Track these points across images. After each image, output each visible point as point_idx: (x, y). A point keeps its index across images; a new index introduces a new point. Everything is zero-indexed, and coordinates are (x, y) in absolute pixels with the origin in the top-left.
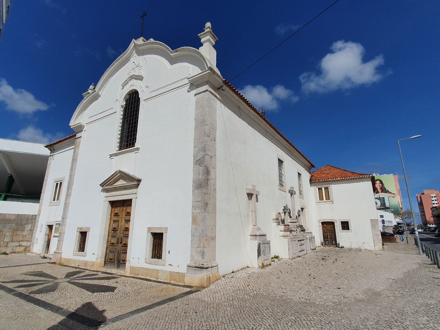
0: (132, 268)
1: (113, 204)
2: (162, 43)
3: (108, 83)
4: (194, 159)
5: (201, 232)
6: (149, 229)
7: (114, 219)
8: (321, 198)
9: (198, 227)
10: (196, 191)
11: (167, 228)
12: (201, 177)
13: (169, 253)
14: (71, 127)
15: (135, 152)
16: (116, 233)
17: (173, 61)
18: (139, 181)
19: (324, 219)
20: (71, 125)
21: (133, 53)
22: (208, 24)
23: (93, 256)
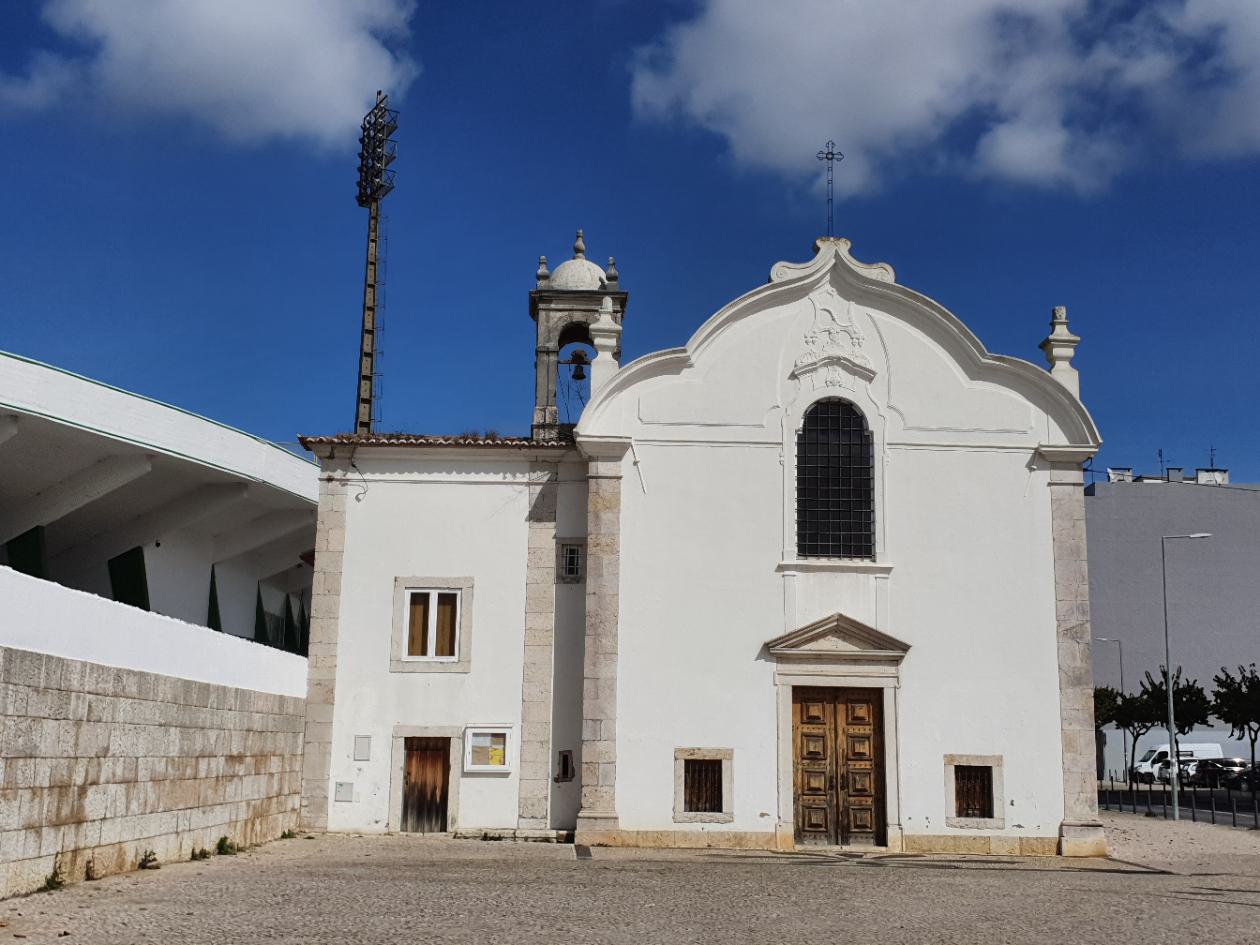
0: (909, 840)
1: (803, 696)
2: (933, 301)
3: (721, 336)
4: (1059, 626)
5: (1086, 766)
6: (949, 758)
7: (805, 730)
8: (418, 646)
9: (1078, 758)
10: (1069, 691)
11: (1000, 758)
12: (1078, 663)
13: (1012, 804)
14: (579, 439)
15: (878, 575)
16: (819, 765)
17: (975, 371)
18: (905, 648)
19: (1002, 783)
20: (581, 433)
21: (824, 281)
22: (1062, 312)
23: (761, 819)
